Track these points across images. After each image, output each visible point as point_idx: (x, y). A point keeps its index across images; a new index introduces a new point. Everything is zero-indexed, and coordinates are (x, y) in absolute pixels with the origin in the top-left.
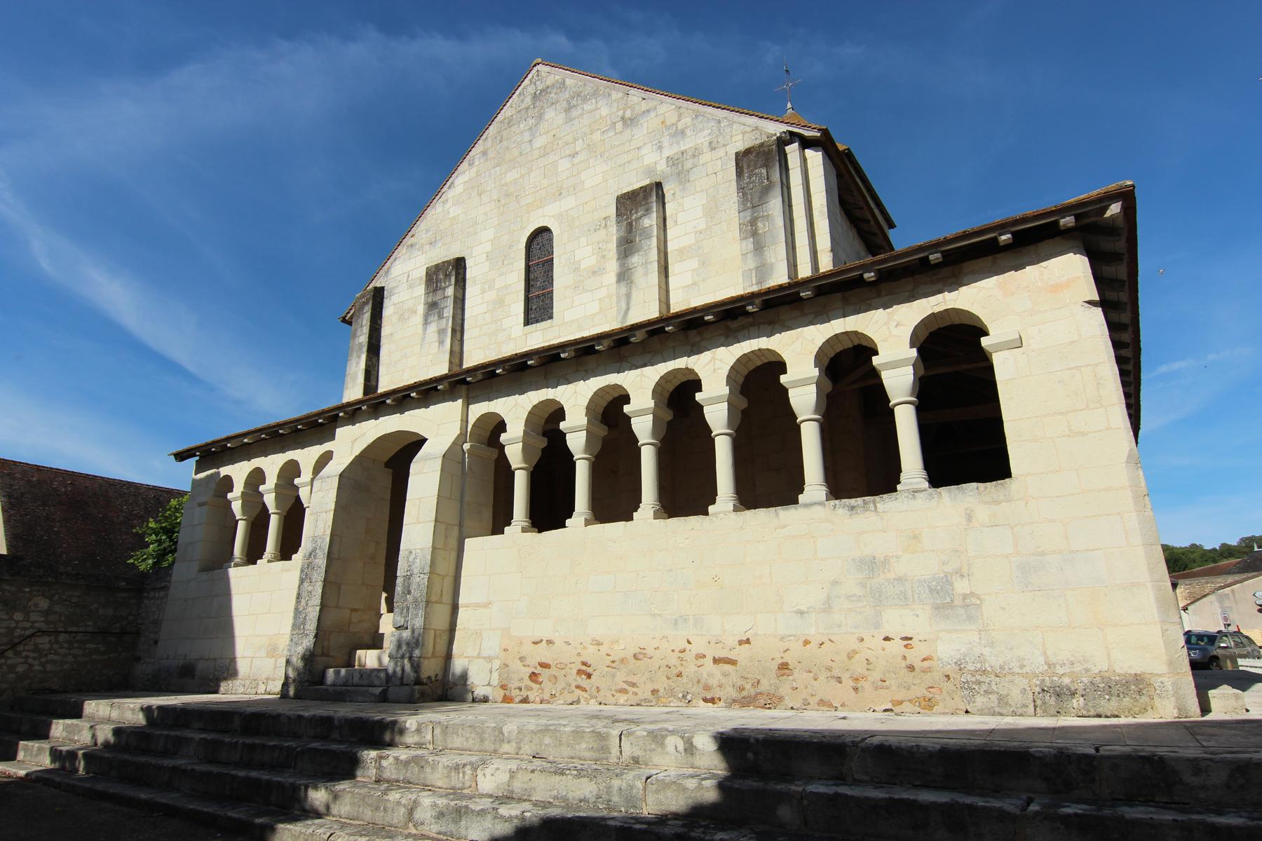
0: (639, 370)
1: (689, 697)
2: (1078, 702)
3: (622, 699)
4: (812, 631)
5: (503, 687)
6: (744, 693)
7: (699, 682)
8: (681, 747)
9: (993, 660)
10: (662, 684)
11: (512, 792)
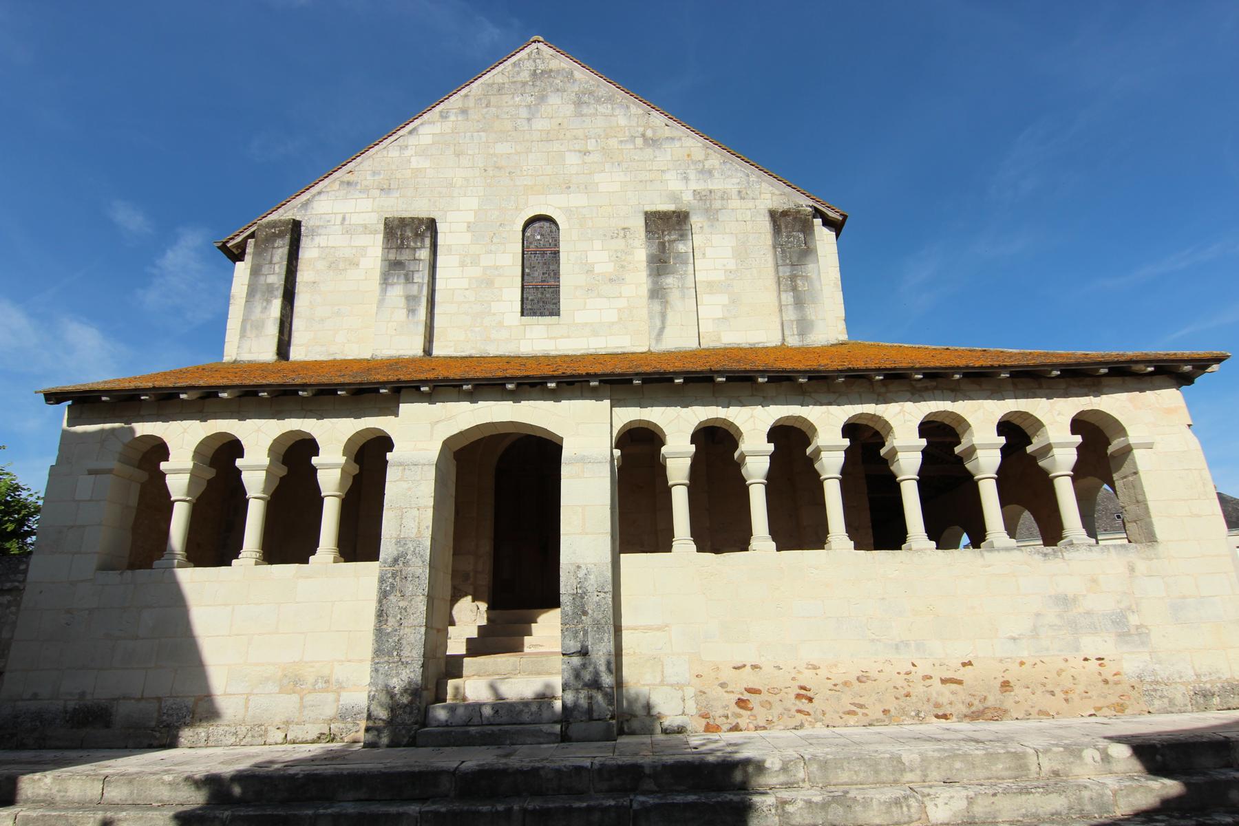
0: (824, 408)
1: (922, 715)
2: (1216, 700)
3: (852, 720)
4: (1025, 654)
6: (974, 709)
7: (928, 700)
8: (1098, 756)
9: (1162, 674)
10: (892, 705)
11: (974, 817)
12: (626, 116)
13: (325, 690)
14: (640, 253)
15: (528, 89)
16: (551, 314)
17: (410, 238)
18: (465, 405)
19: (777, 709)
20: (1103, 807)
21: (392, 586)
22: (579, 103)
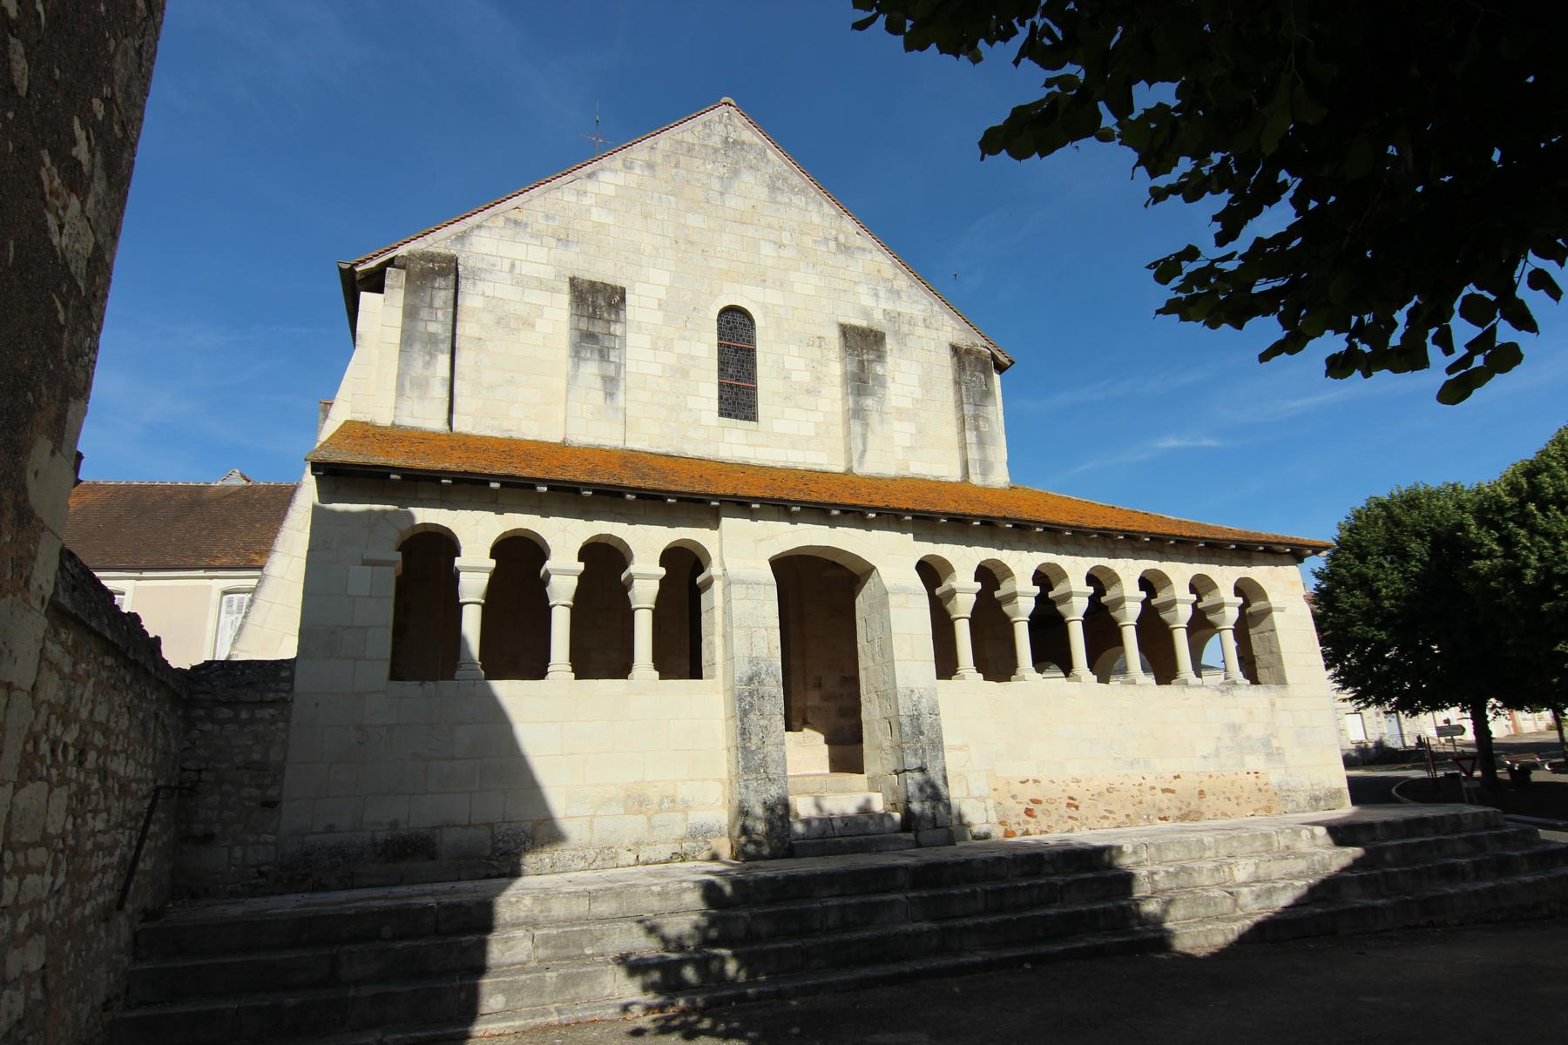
2: (1322, 803)
3: (1106, 823)
5: (1002, 823)
12: (816, 216)
13: (673, 810)
14: (836, 369)
15: (720, 157)
16: (746, 418)
17: (597, 303)
18: (784, 526)
19: (1054, 817)
20: (1325, 867)
21: (751, 705)
22: (773, 188)
